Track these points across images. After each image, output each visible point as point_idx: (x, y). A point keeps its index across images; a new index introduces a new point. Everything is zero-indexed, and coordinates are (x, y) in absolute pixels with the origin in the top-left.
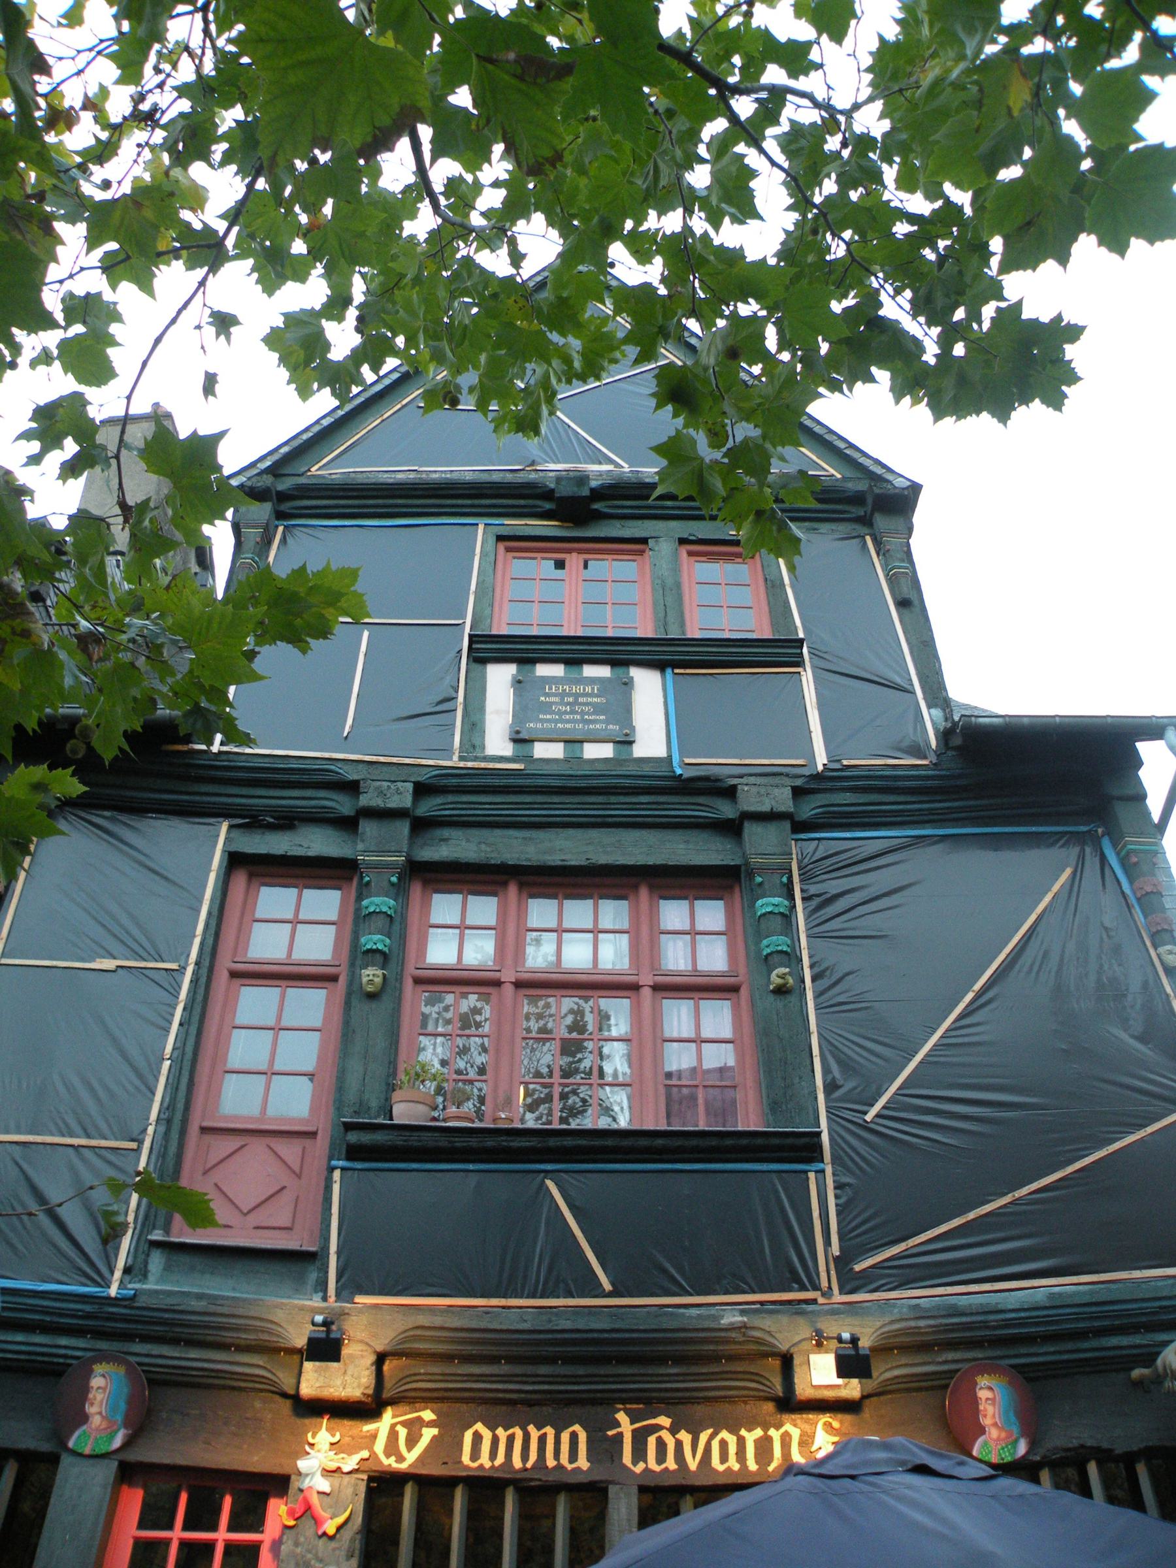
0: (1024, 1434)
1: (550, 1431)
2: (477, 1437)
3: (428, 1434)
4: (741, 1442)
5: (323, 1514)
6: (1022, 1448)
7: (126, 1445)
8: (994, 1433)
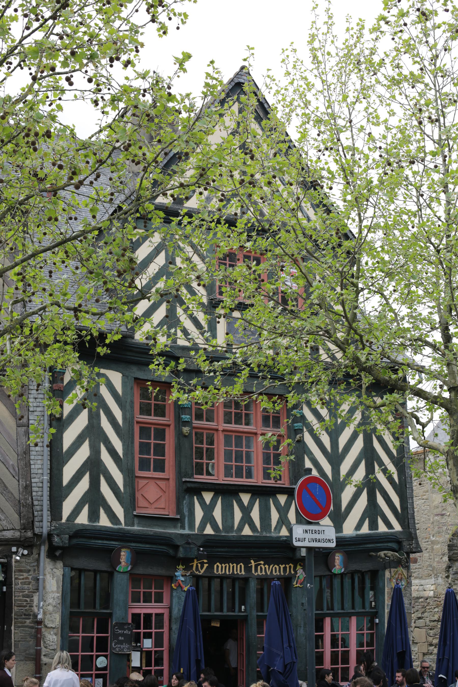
0: (344, 567)
1: (235, 565)
2: (218, 566)
3: (206, 565)
4: (280, 568)
5: (183, 586)
6: (343, 570)
7: (131, 569)
8: (337, 567)
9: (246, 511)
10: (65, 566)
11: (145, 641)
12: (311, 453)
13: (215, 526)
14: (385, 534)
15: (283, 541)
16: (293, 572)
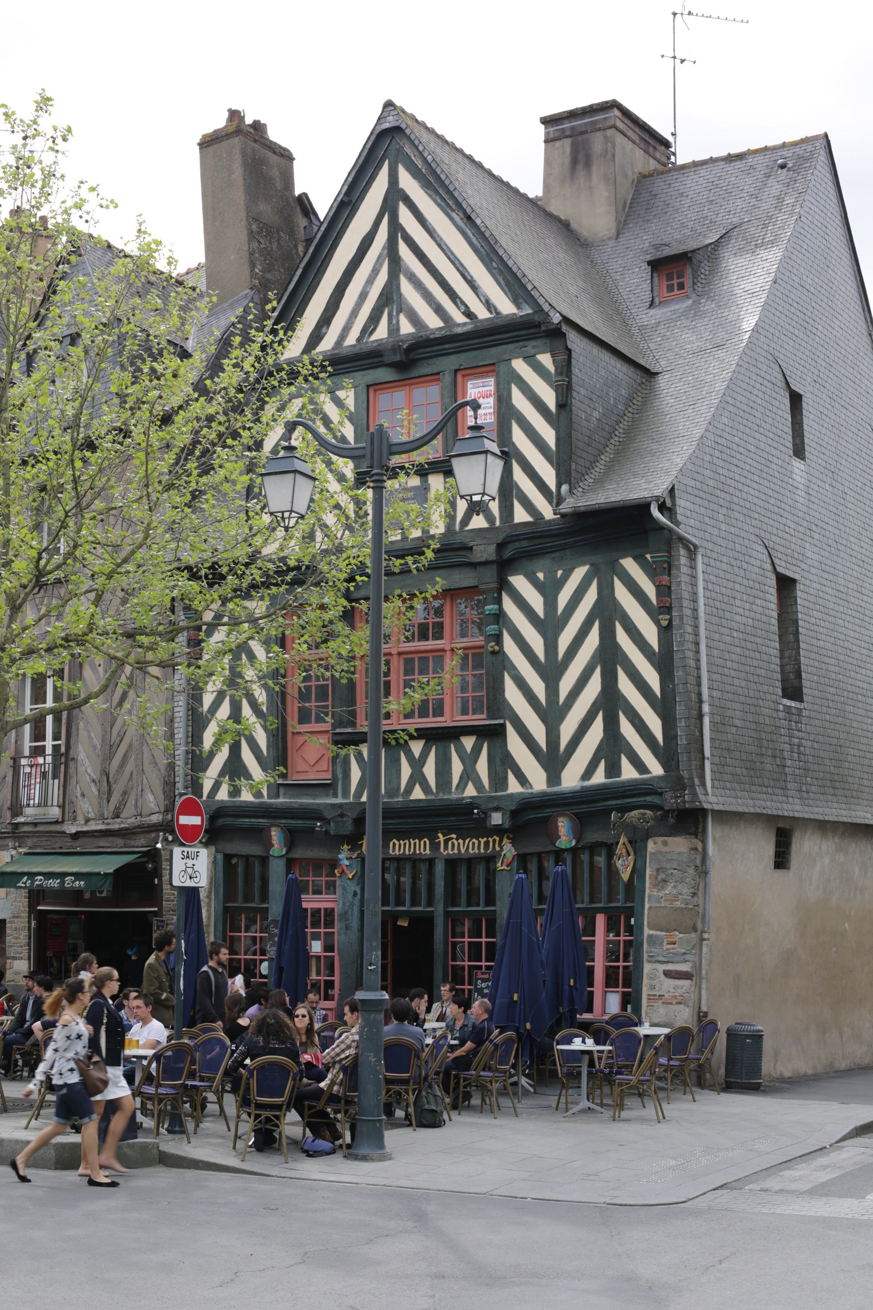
6: (574, 843)
8: (564, 838)
9: (417, 765)
10: (217, 851)
11: (313, 942)
12: (514, 668)
13: (425, 787)
14: (632, 783)
15: (466, 804)
16: (498, 849)
